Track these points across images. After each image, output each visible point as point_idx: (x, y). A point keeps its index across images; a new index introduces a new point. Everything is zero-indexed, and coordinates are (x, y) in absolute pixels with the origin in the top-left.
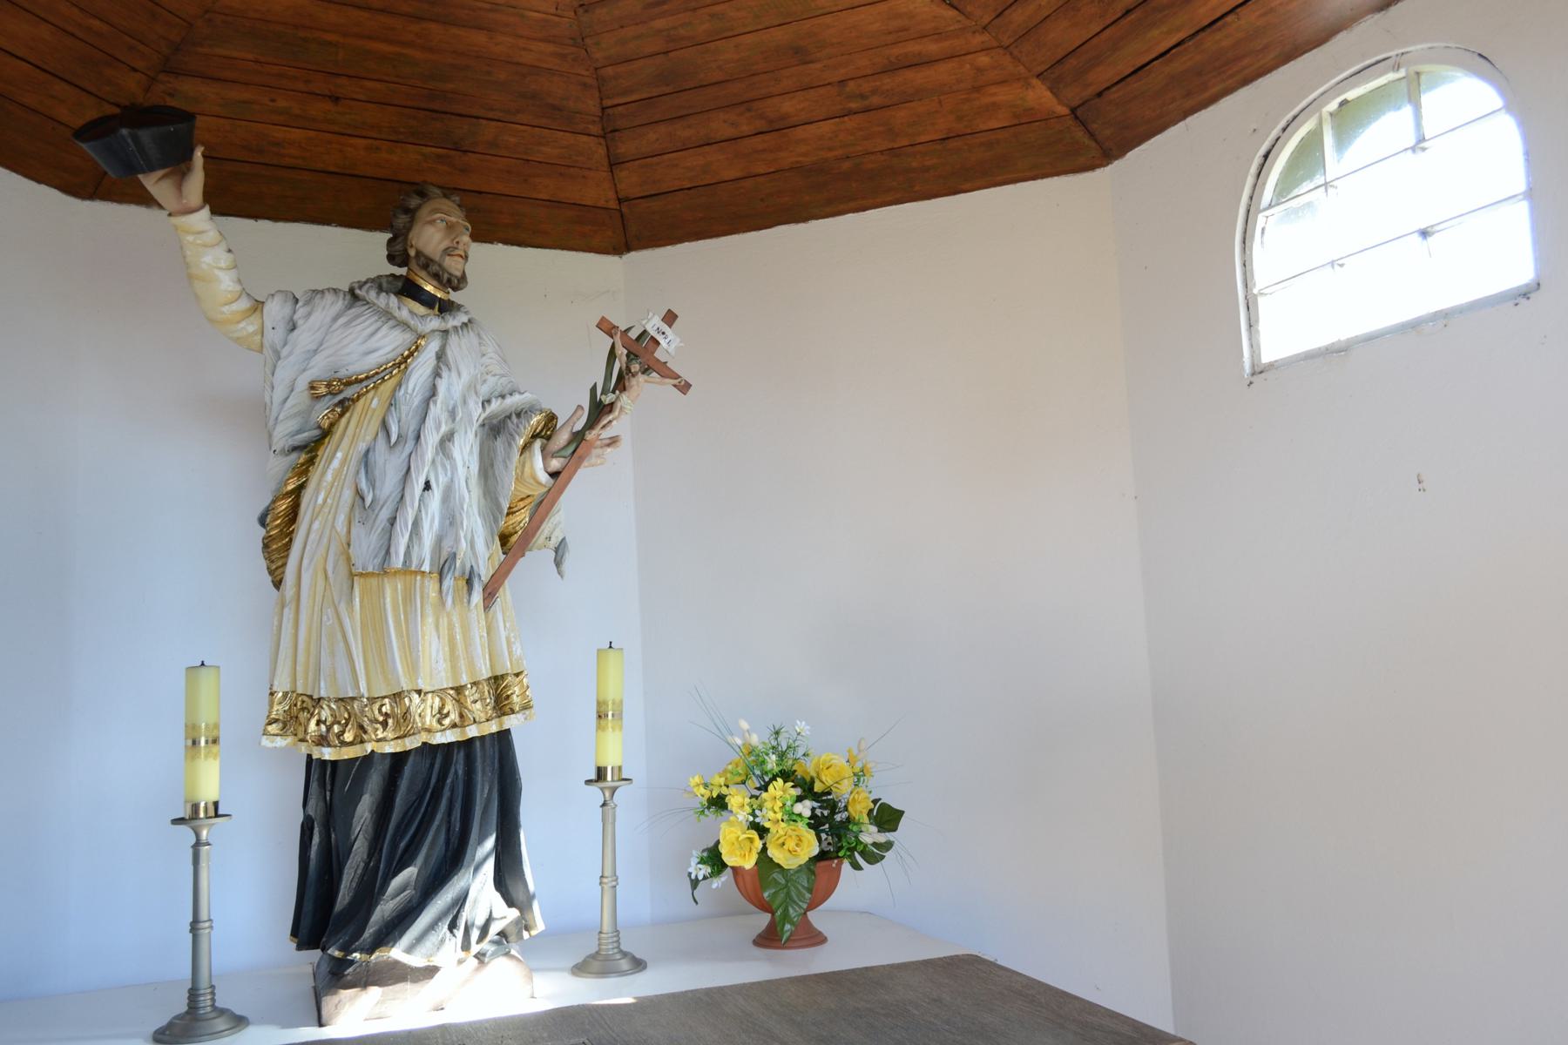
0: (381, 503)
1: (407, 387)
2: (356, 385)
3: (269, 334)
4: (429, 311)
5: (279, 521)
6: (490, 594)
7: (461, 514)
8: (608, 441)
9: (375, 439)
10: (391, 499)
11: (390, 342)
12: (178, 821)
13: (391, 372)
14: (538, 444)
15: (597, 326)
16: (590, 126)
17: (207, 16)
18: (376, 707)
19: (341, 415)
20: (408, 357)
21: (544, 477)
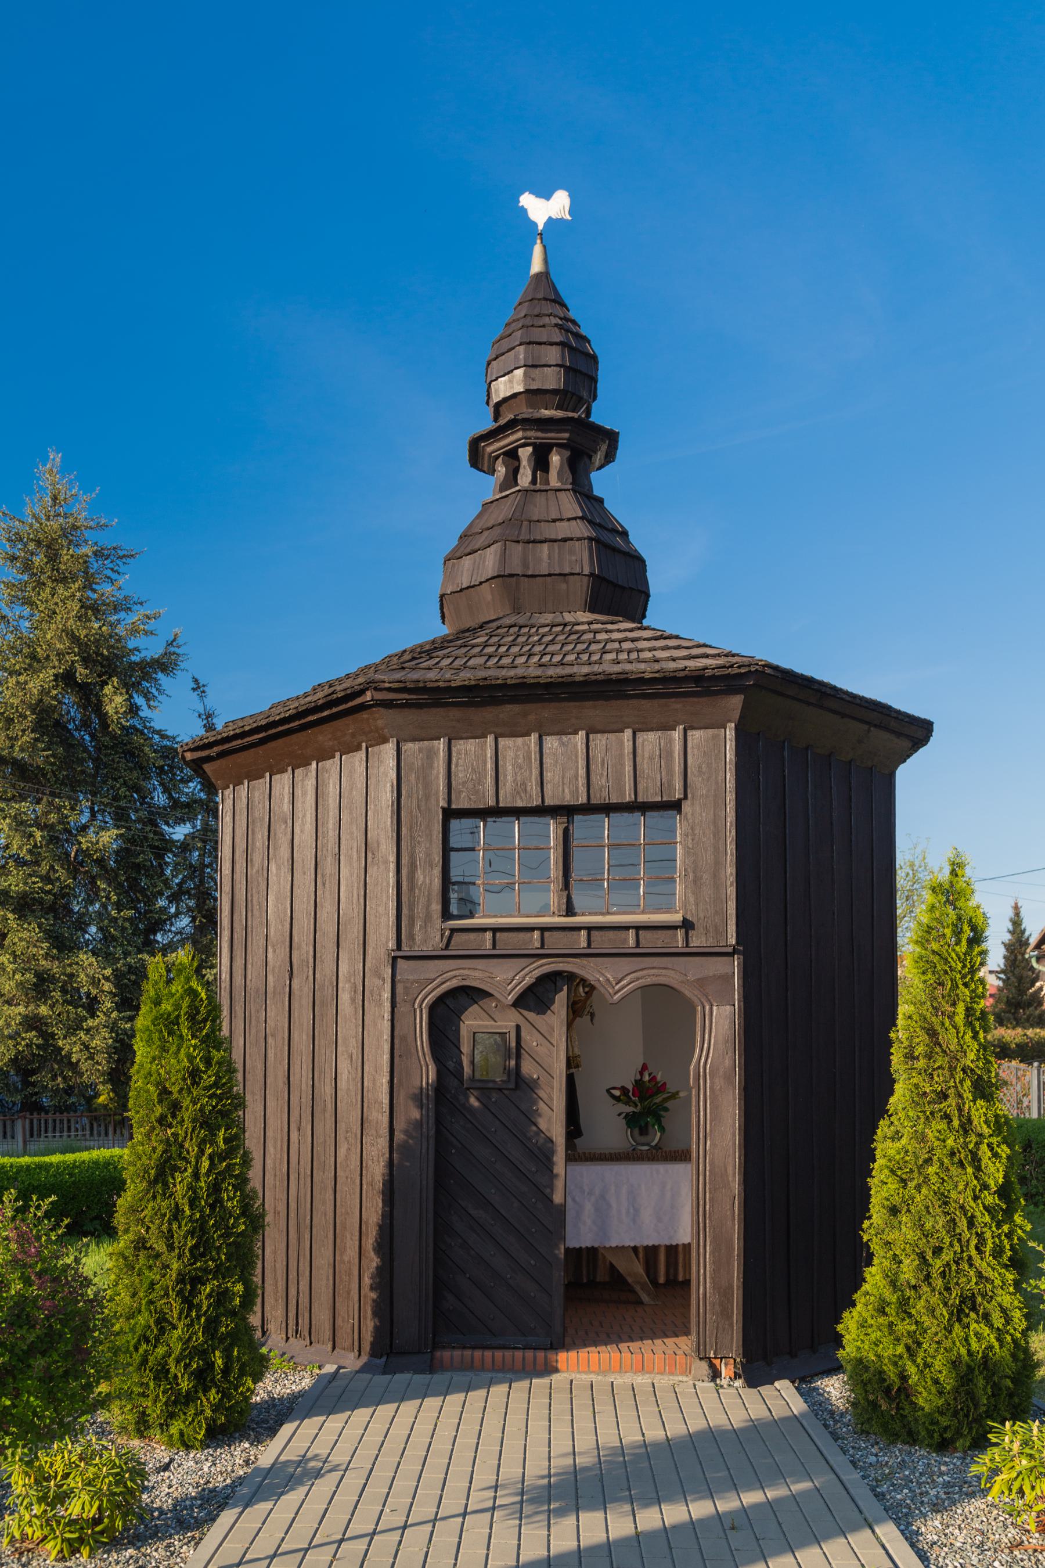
21: (583, 995)
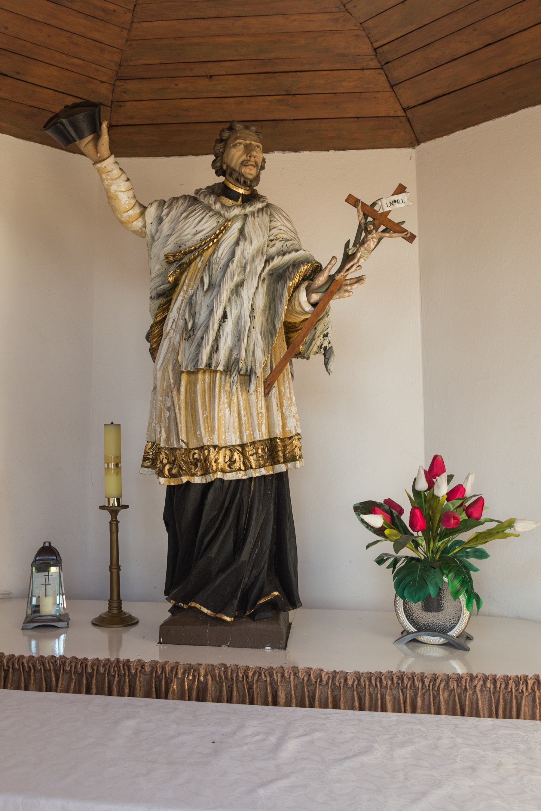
0: (198, 327)
1: (218, 253)
2: (189, 254)
3: (149, 226)
4: (235, 203)
5: (155, 340)
6: (268, 386)
7: (244, 333)
8: (355, 280)
9: (198, 288)
10: (203, 325)
12: (126, 507)
13: (209, 245)
14: (306, 284)
15: (346, 201)
16: (371, 63)
17: (128, 43)
18: (191, 455)
19: (182, 273)
20: (219, 234)
21: (308, 308)
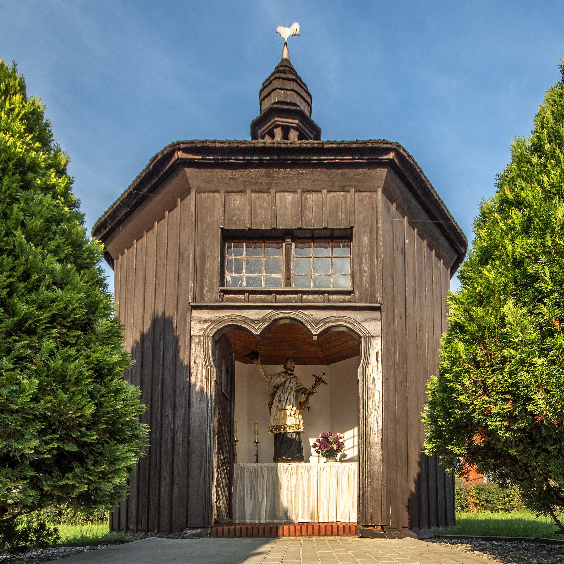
11: (283, 380)
